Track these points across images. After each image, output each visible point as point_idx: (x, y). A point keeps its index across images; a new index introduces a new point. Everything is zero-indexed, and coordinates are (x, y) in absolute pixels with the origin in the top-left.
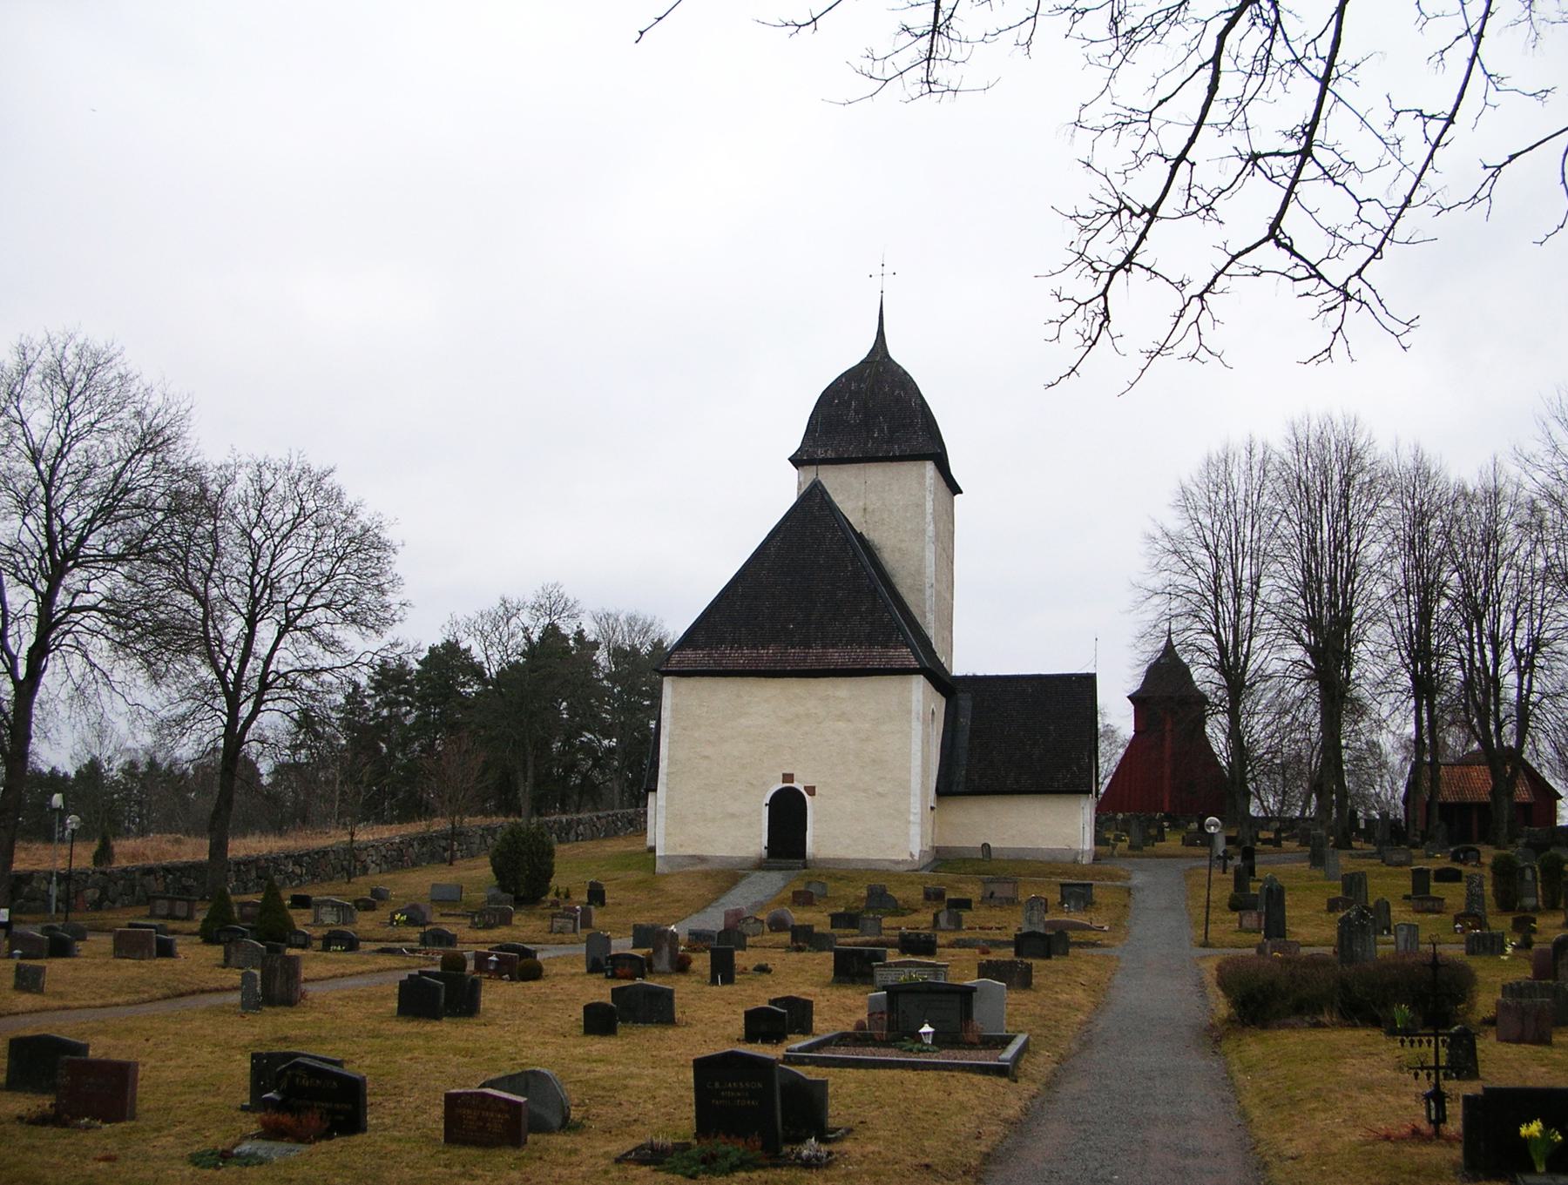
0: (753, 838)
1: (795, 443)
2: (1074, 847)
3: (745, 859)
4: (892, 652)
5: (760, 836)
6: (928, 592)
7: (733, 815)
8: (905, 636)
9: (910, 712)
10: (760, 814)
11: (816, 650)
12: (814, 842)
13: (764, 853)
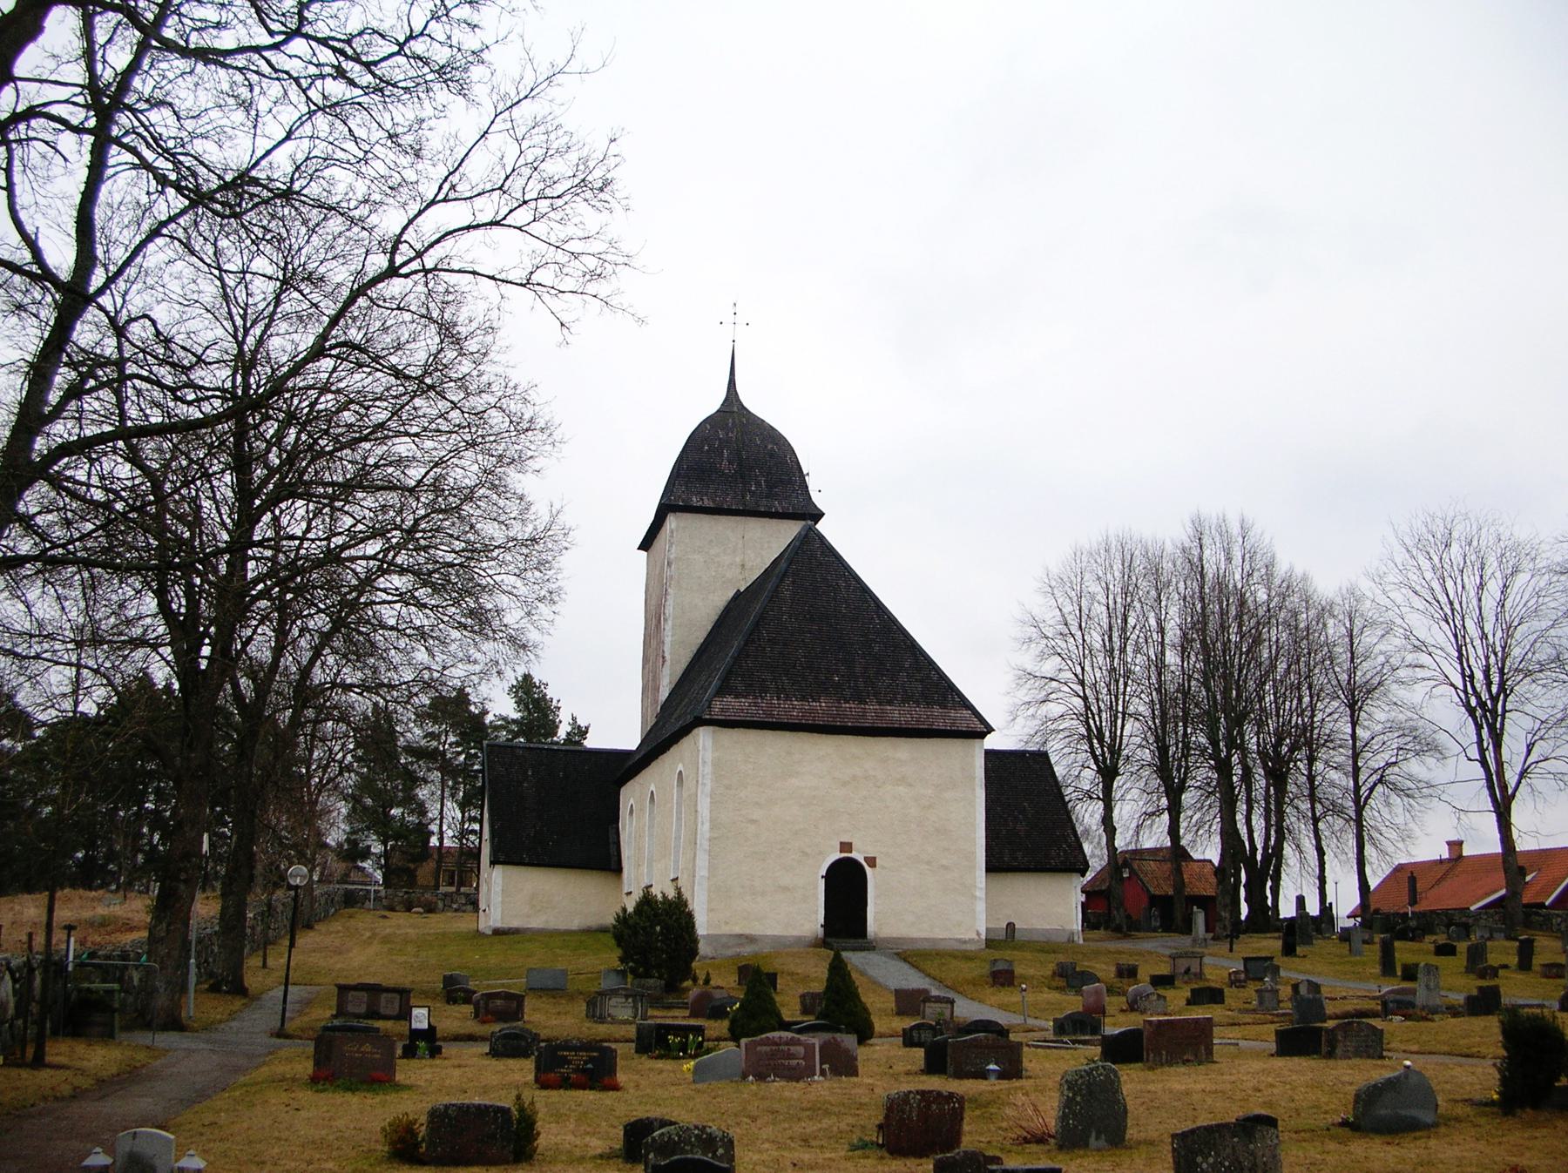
2: (1068, 927)
4: (953, 713)
5: (816, 912)
7: (786, 889)
10: (816, 888)
12: (875, 920)
13: (821, 932)
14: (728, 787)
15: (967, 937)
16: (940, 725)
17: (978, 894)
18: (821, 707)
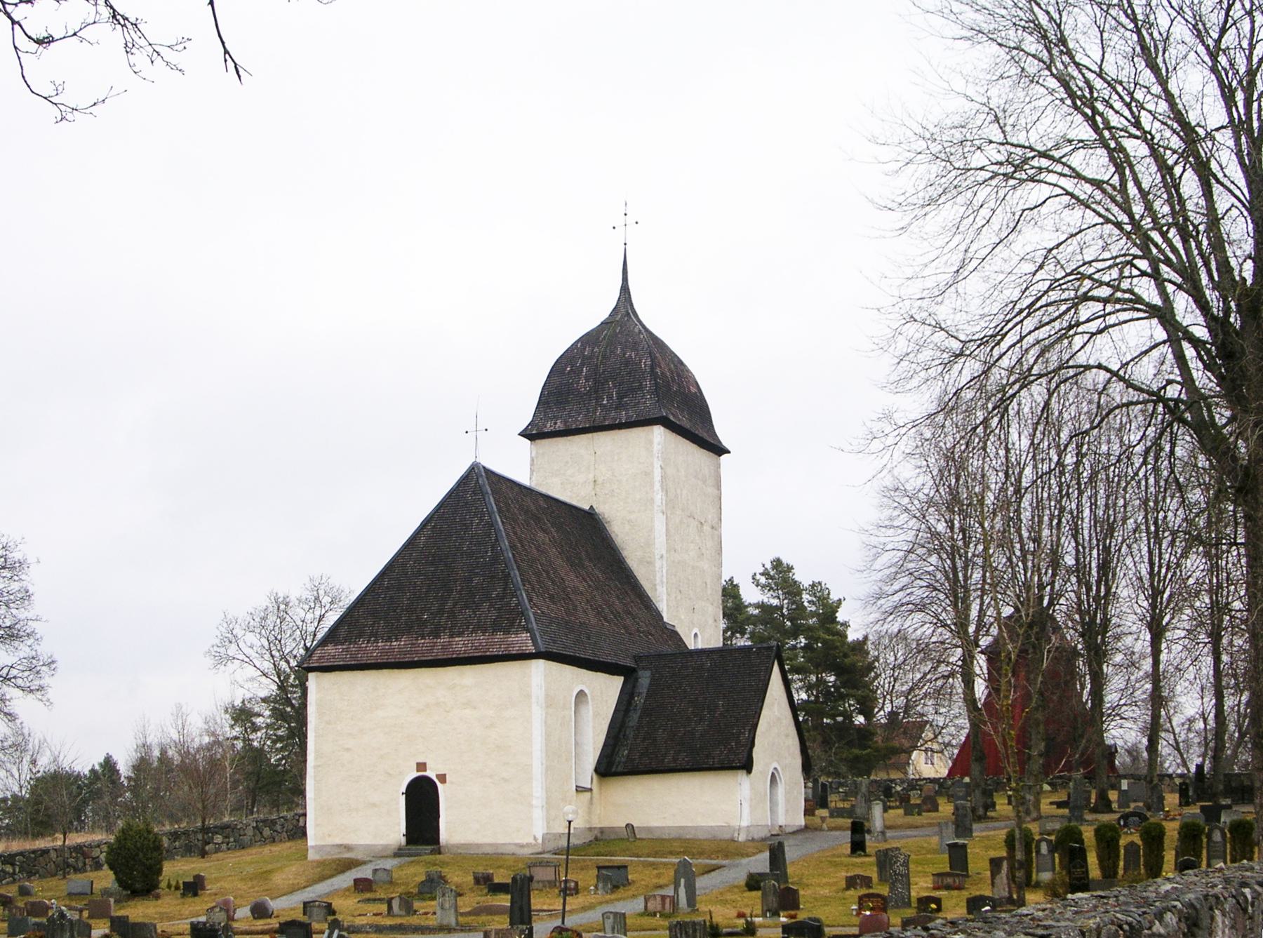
0: (392, 827)
1: (525, 413)
3: (386, 847)
5: (399, 824)
6: (658, 564)
7: (374, 805)
8: (528, 620)
9: (529, 696)
10: (398, 803)
11: (444, 639)
13: (403, 840)
14: (329, 723)
15: (525, 841)
16: (494, 651)
17: (534, 802)
18: (399, 645)
